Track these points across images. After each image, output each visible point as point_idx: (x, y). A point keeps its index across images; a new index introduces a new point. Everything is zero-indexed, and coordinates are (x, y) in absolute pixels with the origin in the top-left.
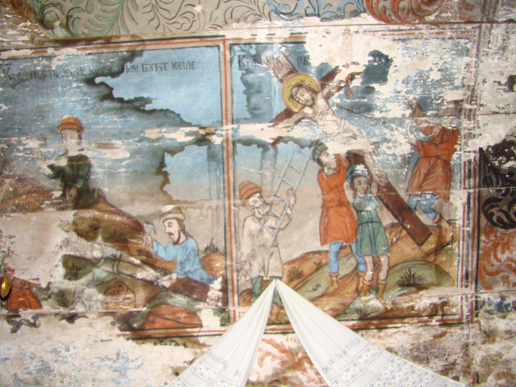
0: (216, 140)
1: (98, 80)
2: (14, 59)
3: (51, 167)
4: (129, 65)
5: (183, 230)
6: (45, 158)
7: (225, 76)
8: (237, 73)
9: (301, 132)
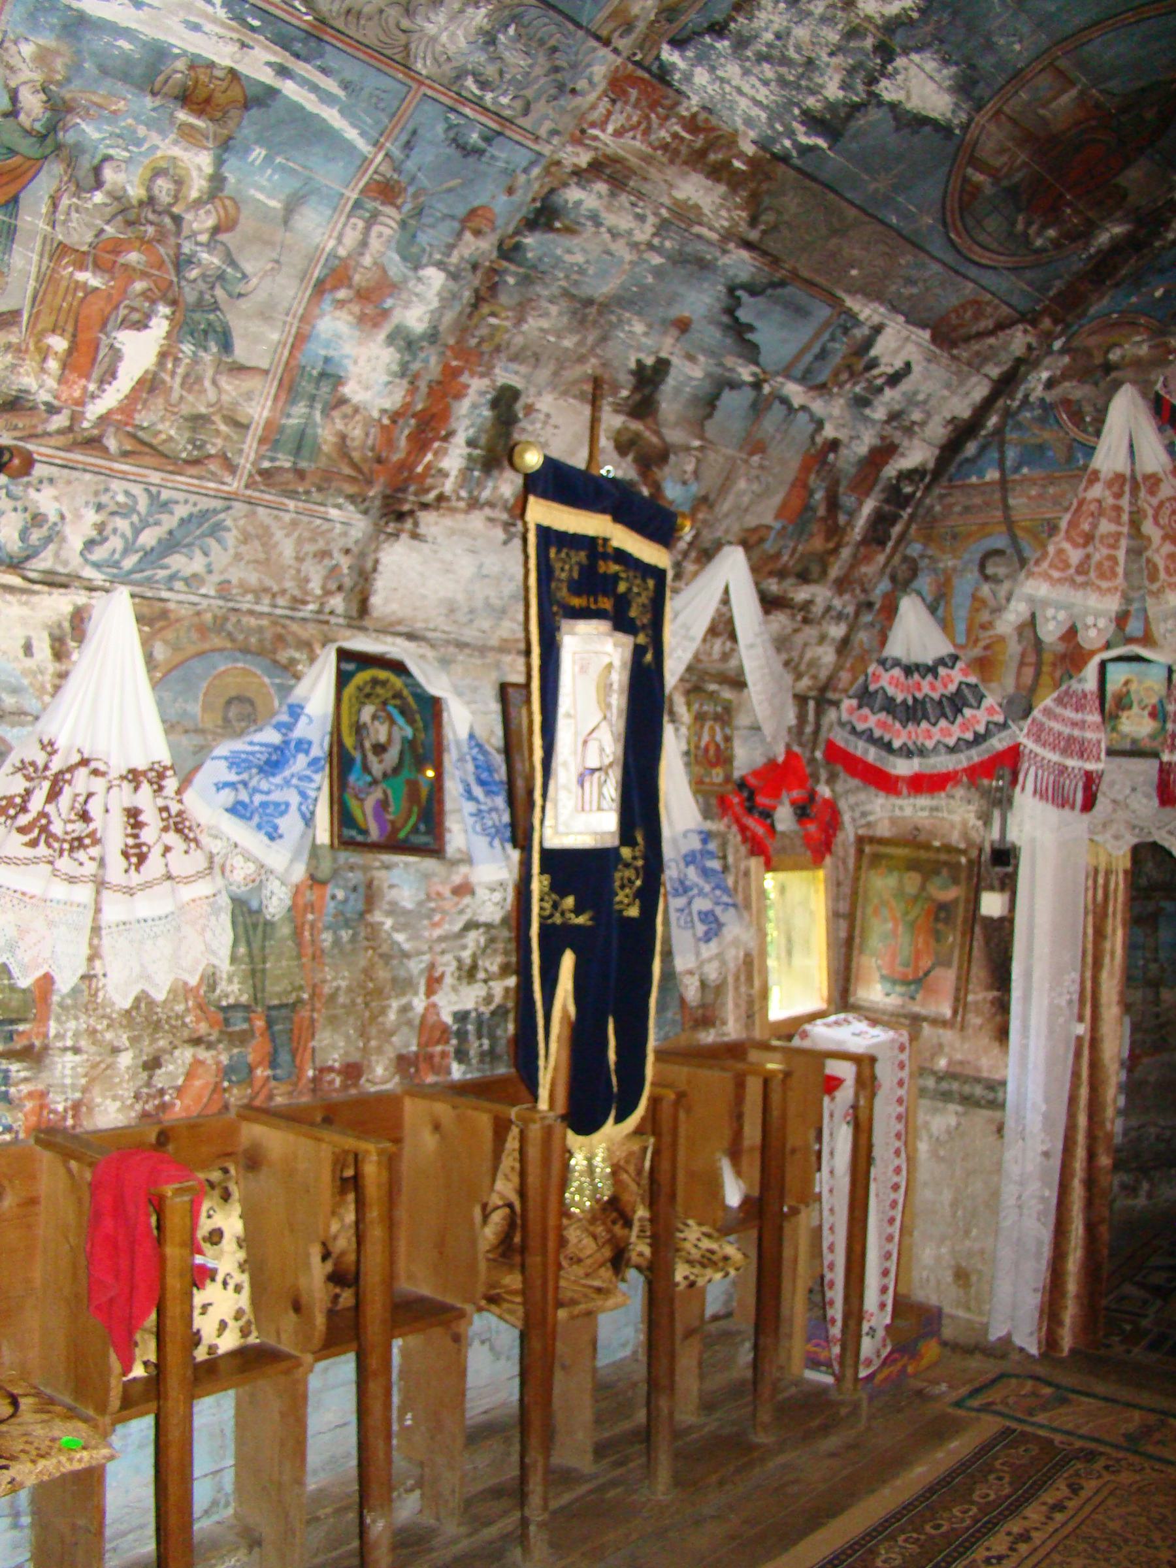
0: (766, 389)
1: (739, 293)
2: (699, 237)
3: (639, 362)
4: (769, 291)
5: (696, 473)
6: (639, 349)
7: (817, 335)
8: (826, 336)
9: (818, 406)
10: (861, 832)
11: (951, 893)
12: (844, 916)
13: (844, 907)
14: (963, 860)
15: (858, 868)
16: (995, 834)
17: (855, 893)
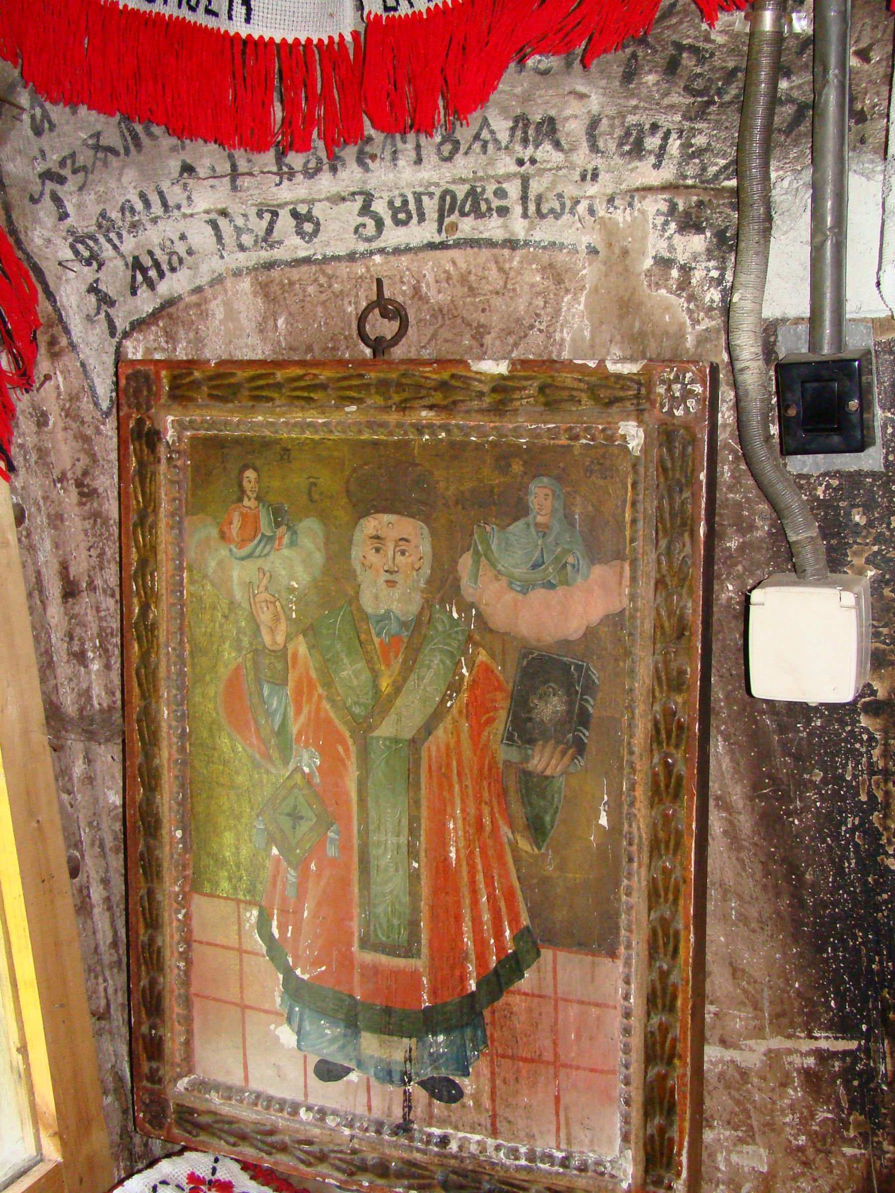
10: (135, 350)
11: (584, 603)
12: (90, 727)
13: (97, 682)
14: (633, 434)
15: (138, 518)
16: (785, 291)
17: (136, 632)
